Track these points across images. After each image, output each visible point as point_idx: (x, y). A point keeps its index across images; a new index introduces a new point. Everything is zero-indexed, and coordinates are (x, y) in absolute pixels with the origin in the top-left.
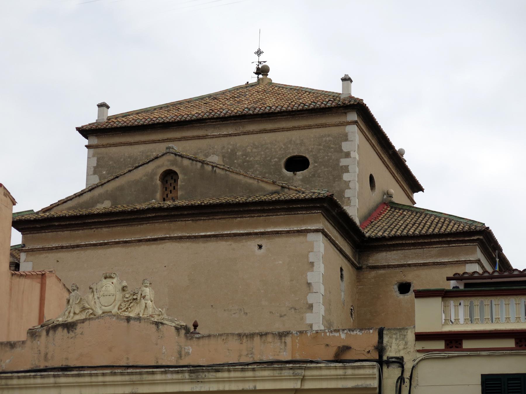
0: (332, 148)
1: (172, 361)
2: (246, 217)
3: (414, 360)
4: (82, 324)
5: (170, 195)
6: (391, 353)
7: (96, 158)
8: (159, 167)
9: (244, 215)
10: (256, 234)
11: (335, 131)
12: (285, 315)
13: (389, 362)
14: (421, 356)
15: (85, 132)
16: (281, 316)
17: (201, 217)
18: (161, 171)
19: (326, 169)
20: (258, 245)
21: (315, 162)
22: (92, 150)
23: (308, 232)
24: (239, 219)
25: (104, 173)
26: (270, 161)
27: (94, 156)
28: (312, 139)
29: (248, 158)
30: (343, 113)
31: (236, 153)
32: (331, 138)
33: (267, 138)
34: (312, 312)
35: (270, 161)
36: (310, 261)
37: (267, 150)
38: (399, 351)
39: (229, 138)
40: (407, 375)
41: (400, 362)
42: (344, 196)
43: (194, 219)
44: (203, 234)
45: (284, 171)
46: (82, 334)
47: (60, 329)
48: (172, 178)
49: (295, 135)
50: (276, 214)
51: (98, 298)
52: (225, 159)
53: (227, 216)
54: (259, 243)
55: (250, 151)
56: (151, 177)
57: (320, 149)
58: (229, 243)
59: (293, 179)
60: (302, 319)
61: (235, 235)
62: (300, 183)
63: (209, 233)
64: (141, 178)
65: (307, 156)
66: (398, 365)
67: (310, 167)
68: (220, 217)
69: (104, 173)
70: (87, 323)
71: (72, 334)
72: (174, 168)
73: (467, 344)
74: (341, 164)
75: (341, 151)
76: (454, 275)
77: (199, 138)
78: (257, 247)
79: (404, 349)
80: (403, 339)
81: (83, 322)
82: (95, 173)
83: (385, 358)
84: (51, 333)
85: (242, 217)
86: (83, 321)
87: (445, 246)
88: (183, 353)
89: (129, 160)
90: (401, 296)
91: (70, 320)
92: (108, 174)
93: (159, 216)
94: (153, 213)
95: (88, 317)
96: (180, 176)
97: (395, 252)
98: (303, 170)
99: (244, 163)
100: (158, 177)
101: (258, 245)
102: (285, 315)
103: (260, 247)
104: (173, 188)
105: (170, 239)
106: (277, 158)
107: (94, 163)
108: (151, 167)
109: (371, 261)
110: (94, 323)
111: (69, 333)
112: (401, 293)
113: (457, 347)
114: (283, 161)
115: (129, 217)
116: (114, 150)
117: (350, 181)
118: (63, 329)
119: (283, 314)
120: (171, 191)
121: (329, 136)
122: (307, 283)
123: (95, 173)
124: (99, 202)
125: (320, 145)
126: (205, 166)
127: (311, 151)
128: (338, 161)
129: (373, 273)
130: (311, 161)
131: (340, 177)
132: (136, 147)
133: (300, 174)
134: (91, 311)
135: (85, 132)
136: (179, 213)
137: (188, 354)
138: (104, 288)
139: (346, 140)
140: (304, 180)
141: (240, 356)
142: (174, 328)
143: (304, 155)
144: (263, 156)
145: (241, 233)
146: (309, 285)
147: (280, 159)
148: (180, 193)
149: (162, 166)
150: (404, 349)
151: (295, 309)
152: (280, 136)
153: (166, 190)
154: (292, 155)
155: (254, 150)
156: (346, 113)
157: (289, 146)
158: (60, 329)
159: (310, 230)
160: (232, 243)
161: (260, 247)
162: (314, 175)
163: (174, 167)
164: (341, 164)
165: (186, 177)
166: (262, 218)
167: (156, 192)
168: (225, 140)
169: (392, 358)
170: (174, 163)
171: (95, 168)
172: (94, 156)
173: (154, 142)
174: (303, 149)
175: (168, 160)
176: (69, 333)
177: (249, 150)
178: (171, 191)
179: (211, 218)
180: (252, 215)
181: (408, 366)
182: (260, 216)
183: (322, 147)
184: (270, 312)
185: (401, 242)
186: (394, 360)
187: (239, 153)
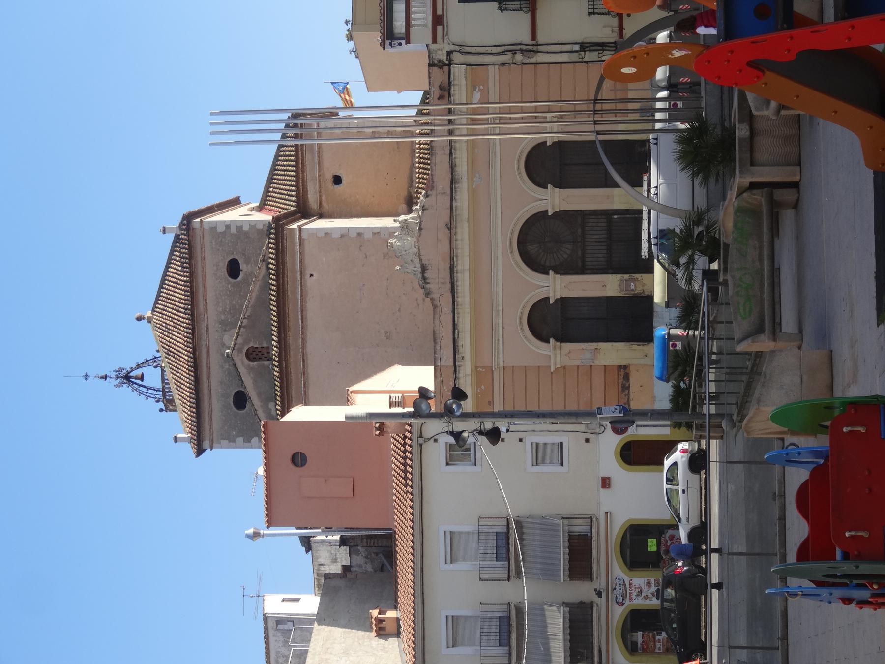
0: (222, 240)
1: (448, 198)
2: (288, 288)
3: (449, 44)
4: (423, 260)
5: (266, 355)
6: (444, 58)
7: (221, 441)
8: (243, 364)
9: (286, 289)
10: (301, 279)
11: (207, 238)
12: (365, 254)
13: (450, 60)
14: (446, 41)
15: (200, 451)
16: (366, 257)
17: (286, 323)
18: (246, 362)
19: (239, 244)
20: (310, 277)
21: (233, 253)
22: (214, 445)
23: (301, 238)
24: (289, 293)
25: (234, 433)
26: (230, 291)
27: (220, 443)
28: (214, 256)
29: (227, 310)
30: (193, 232)
31: (222, 320)
32: (214, 241)
33: (210, 295)
34: (364, 233)
35: (230, 291)
36: (323, 235)
37: (221, 294)
38: (443, 54)
39: (210, 326)
40: (458, 48)
41: (449, 53)
42: (262, 230)
43: (288, 330)
44: (300, 321)
45: (239, 279)
46: (429, 260)
47: (426, 275)
48: (252, 354)
49: (210, 270)
50: (286, 264)
51: (405, 251)
52: (227, 329)
53: (287, 303)
54: (309, 276)
55: (221, 309)
56: (250, 369)
57: (222, 249)
58: (308, 301)
59: (246, 272)
60: (368, 241)
61: (302, 296)
62: (249, 266)
63: (300, 317)
64: (252, 378)
65: (228, 260)
66: (451, 55)
67: (236, 258)
68: (287, 308)
69: (234, 433)
70: (422, 257)
71: (429, 267)
72: (245, 351)
73: (439, 12)
74: (235, 232)
75: (224, 232)
76: (381, 46)
77: (208, 352)
78: (312, 278)
79: (442, 51)
80: (436, 51)
81: (422, 259)
82: (234, 441)
83: (447, 63)
84: (428, 281)
85: (288, 290)
86: (421, 260)
87: (304, 148)
88: (443, 192)
89: (224, 412)
90: (344, 182)
91: (420, 270)
92: (235, 429)
93: (285, 358)
94: (282, 362)
95: (418, 258)
96: (251, 345)
97: (308, 188)
98: (239, 264)
99: (231, 313)
100: (251, 364)
101: (310, 277)
102: (365, 254)
103: (311, 275)
104: (260, 353)
105: (304, 347)
106: (228, 285)
107: (225, 442)
108: (242, 370)
109: (315, 207)
110: (422, 252)
111: (428, 269)
112: (341, 183)
113: (441, 18)
114: (230, 279)
115: (285, 383)
116: (215, 426)
117: (250, 225)
118: (425, 273)
119: (364, 256)
120: (262, 354)
121: (212, 243)
122: (341, 237)
123: (234, 441)
124: (270, 413)
125: (219, 250)
126: (243, 325)
127: (224, 257)
128: (232, 235)
129: (325, 204)
130: (231, 257)
131: (246, 233)
132: (213, 406)
133: (243, 266)
134: (414, 256)
135: (200, 451)
136: (283, 341)
137: (443, 188)
138: (399, 248)
139: (215, 228)
140: (247, 262)
141: (445, 154)
142: (427, 199)
143: (227, 263)
144: (226, 297)
145: (301, 291)
146: (342, 236)
147: (229, 283)
148: (265, 345)
149: (242, 360)
150: (442, 51)
151: (361, 246)
152: (210, 282)
153: (261, 358)
154: (226, 273)
155: (221, 305)
156: (193, 229)
157: (218, 275)
158: (426, 275)
159: (299, 235)
160: (308, 298)
161: (311, 275)
162: (244, 254)
163: (244, 350)
164: (235, 232)
165: (253, 340)
166: (288, 275)
167: (264, 364)
168: (211, 330)
169: (447, 58)
170: (240, 351)
171: (230, 441)
172: (220, 443)
173: (210, 391)
174: (221, 264)
175: (238, 355)
176: (428, 269)
177: (220, 309)
178: (262, 354)
179: (287, 316)
180: (286, 282)
181: (452, 48)
182: (287, 276)
183: (221, 249)
184: (363, 266)
185: (301, 182)
186: (448, 57)
187: (223, 317)
